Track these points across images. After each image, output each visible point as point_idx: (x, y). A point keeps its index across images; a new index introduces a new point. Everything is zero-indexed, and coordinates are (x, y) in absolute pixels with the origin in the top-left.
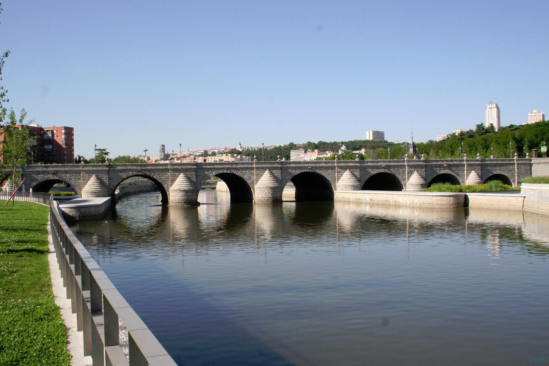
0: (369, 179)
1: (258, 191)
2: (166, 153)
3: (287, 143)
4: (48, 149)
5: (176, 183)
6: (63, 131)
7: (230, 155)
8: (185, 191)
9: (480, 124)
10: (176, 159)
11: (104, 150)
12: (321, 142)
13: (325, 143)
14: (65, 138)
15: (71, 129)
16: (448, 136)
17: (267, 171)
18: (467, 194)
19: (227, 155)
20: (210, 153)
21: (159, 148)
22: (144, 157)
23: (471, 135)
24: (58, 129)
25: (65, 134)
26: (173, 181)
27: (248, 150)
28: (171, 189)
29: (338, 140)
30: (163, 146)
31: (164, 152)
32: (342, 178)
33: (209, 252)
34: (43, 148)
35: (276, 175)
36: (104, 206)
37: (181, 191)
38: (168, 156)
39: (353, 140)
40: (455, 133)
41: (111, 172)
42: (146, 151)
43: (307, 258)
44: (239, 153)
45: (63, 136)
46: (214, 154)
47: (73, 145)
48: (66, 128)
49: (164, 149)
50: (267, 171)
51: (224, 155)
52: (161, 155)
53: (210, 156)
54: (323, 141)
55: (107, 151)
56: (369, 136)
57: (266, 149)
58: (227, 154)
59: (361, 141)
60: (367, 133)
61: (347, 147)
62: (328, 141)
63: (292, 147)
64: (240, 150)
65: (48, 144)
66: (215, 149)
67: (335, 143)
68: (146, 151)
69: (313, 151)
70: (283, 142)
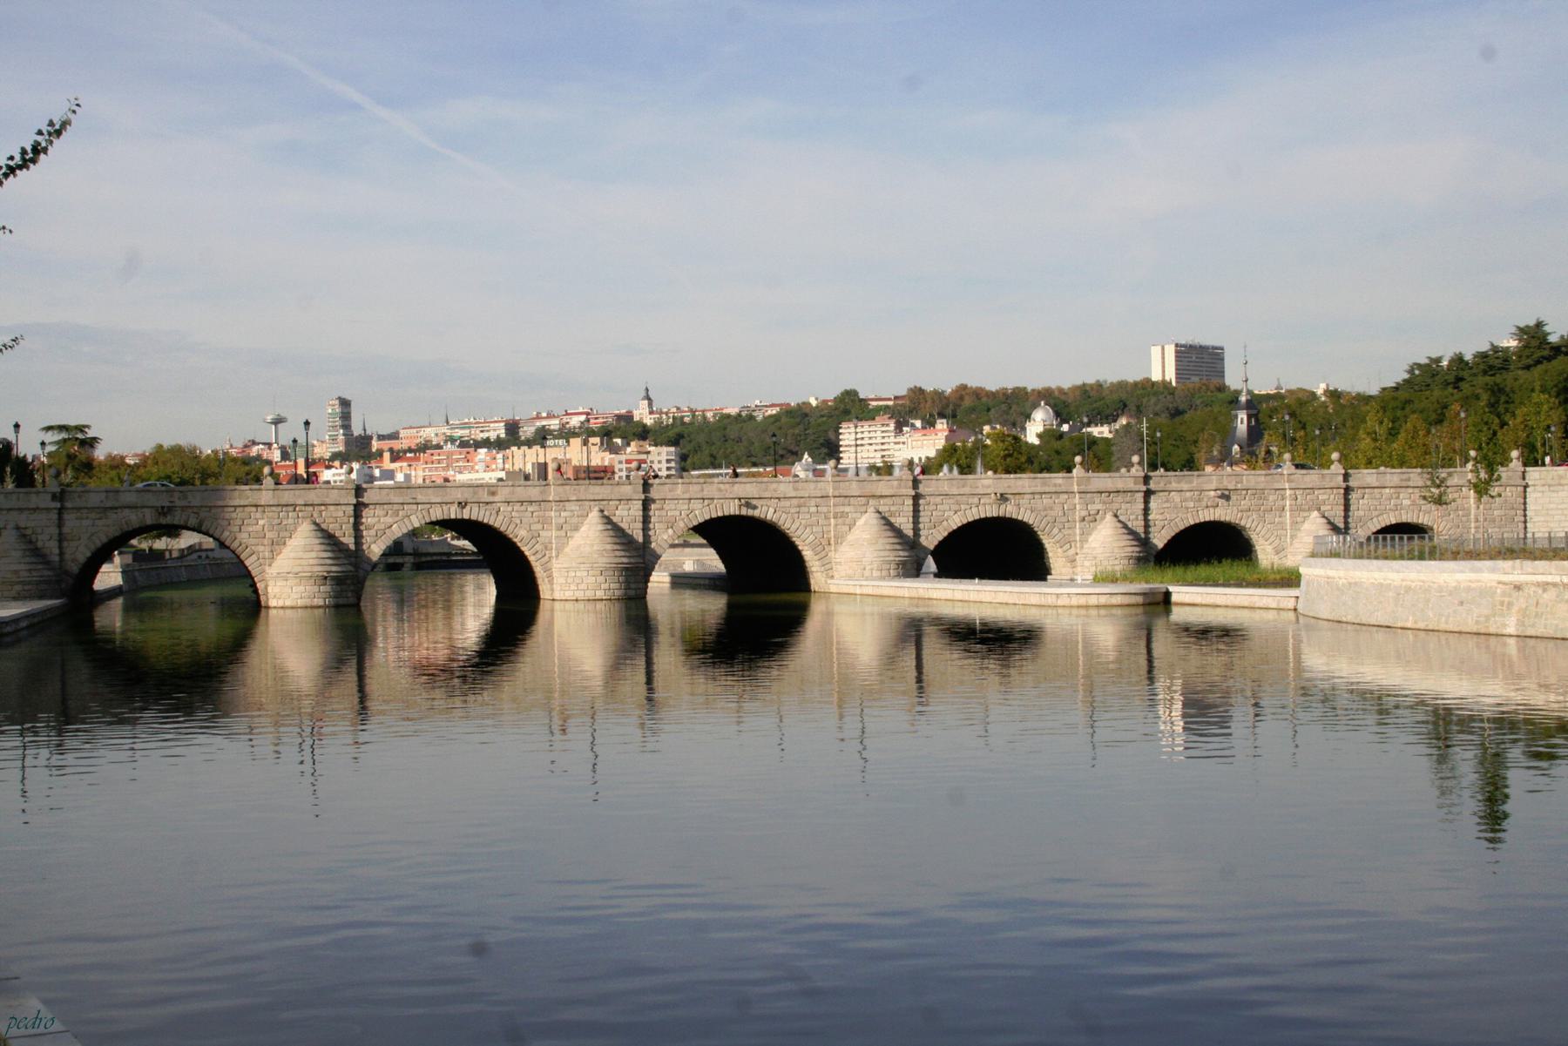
0: (946, 539)
1: (562, 580)
2: (357, 430)
3: (831, 393)
7: (597, 440)
9: (1532, 323)
10: (387, 455)
11: (80, 428)
12: (964, 387)
13: (978, 393)
16: (1411, 371)
18: (1171, 589)
19: (585, 443)
20: (527, 431)
21: (333, 408)
22: (269, 445)
23: (1493, 363)
26: (277, 544)
27: (678, 421)
28: (271, 571)
29: (1033, 383)
32: (850, 537)
33: (70, 758)
36: (907, 602)
38: (365, 440)
39: (1091, 380)
40: (1438, 360)
41: (66, 516)
43: (717, 736)
44: (643, 433)
46: (542, 437)
49: (346, 417)
51: (576, 442)
53: (529, 443)
54: (973, 383)
55: (91, 434)
56: (1162, 367)
57: (751, 418)
58: (586, 433)
59: (1122, 385)
60: (1155, 352)
61: (1061, 414)
62: (992, 387)
63: (852, 407)
64: (649, 421)
66: (550, 416)
67: (798, 415)
68: (278, 421)
69: (929, 423)
70: (816, 392)
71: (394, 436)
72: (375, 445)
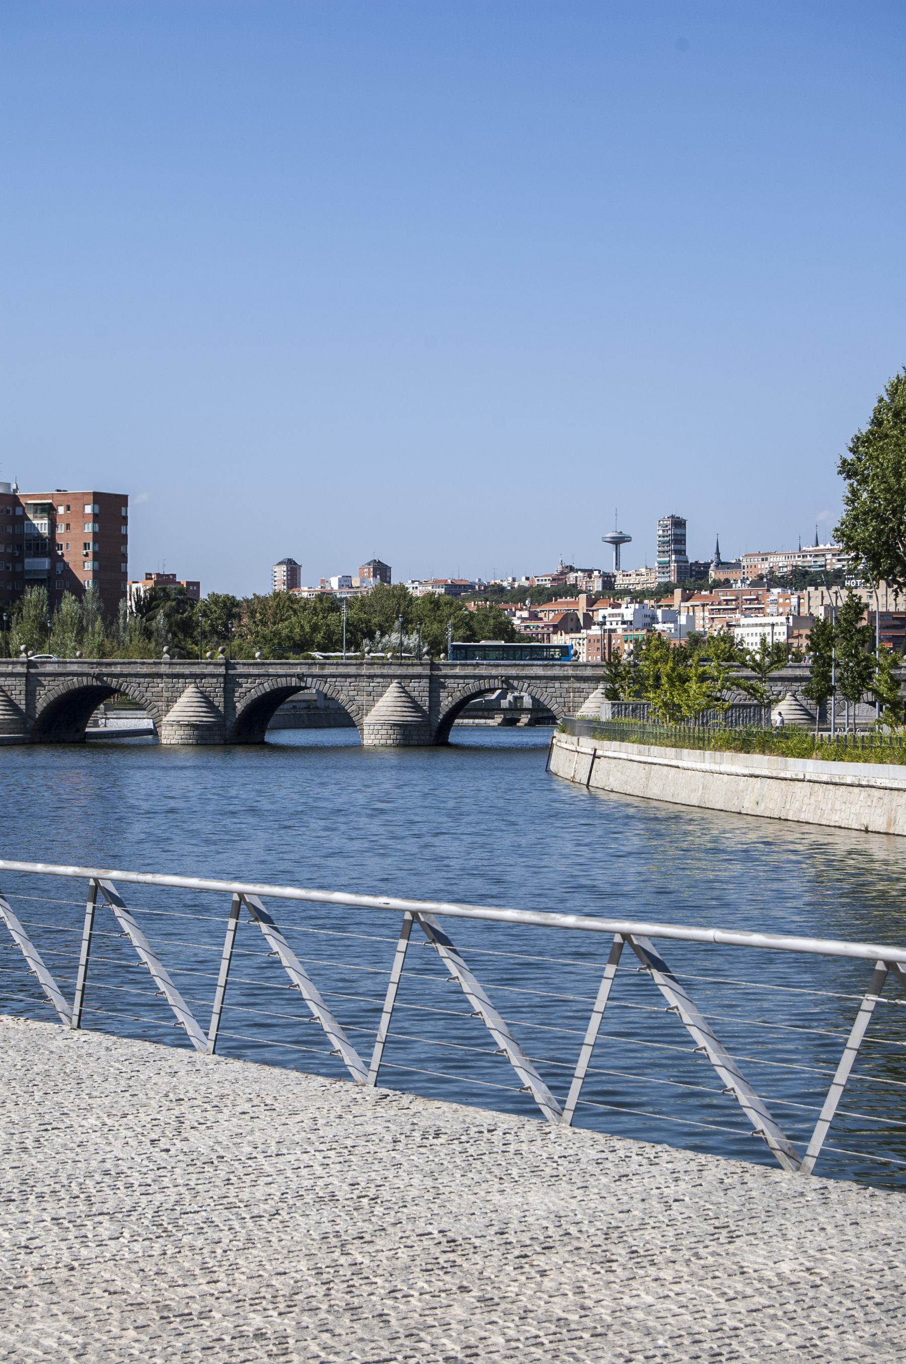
4: (36, 572)
5: (176, 707)
6: (88, 509)
8: (194, 726)
14: (95, 534)
15: (122, 500)
17: (394, 684)
24: (73, 501)
25: (96, 517)
26: (171, 701)
30: (679, 523)
31: (680, 552)
34: (18, 568)
35: (413, 694)
37: (181, 725)
42: (618, 541)
45: (89, 528)
47: (124, 558)
48: (99, 498)
50: (394, 684)
52: (664, 566)
65: (36, 555)
68: (618, 541)
71: (737, 565)
72: (713, 574)
